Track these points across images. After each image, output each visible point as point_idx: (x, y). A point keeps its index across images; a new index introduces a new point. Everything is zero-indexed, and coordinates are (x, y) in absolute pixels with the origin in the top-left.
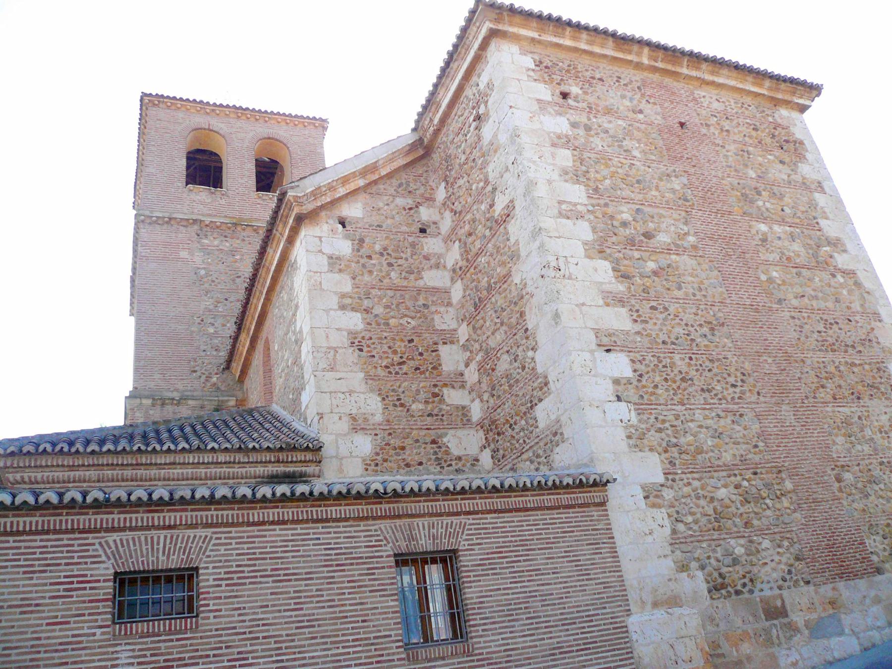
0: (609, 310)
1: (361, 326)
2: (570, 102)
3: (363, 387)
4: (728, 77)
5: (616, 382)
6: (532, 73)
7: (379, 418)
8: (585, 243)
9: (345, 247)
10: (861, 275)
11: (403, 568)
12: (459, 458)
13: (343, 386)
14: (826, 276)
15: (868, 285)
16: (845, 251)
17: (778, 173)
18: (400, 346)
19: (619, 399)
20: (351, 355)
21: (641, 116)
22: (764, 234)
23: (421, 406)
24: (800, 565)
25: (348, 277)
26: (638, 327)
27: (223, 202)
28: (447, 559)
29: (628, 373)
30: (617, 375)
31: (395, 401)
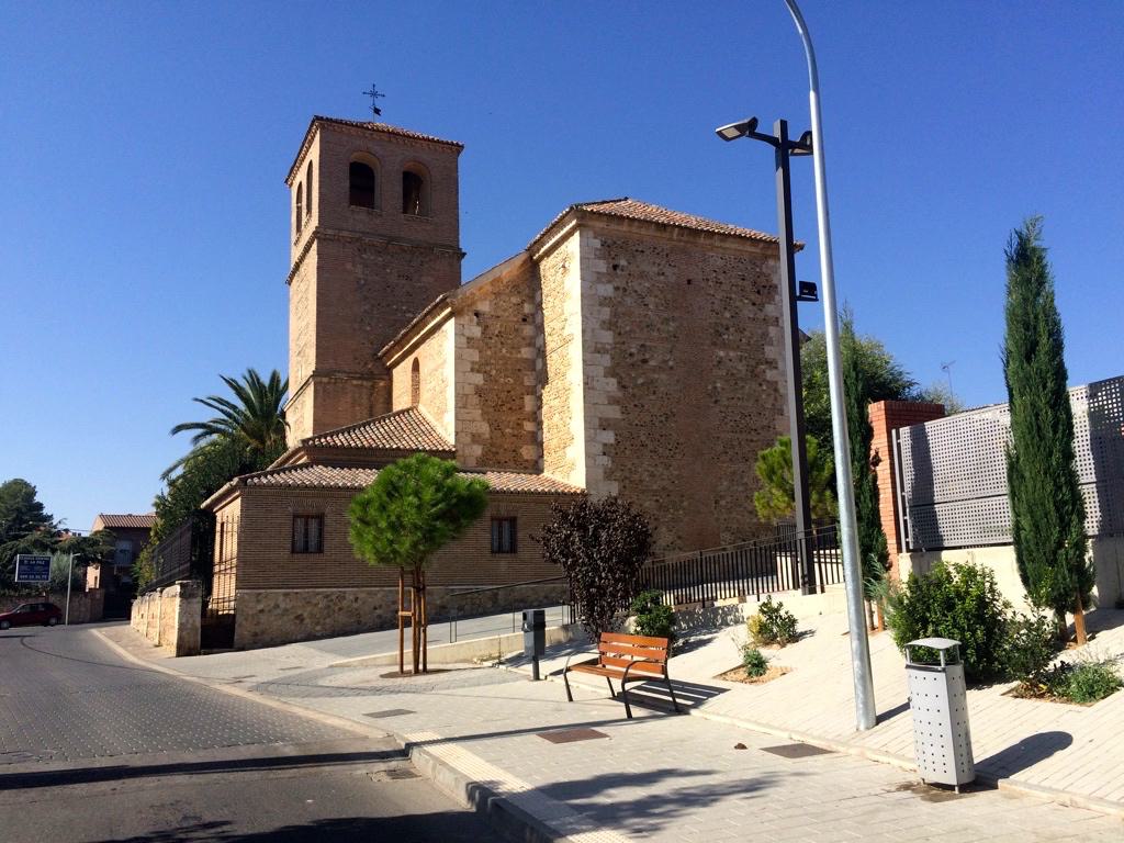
0: (610, 407)
1: (482, 382)
2: (618, 271)
3: (479, 418)
4: (733, 243)
5: (605, 445)
6: (598, 253)
7: (487, 436)
8: (605, 368)
9: (477, 332)
10: (780, 386)
11: (937, 498)
12: (527, 461)
13: (468, 417)
14: (755, 386)
15: (782, 391)
16: (776, 368)
17: (748, 311)
18: (503, 395)
19: (604, 454)
20: (475, 400)
21: (662, 277)
22: (721, 358)
23: (510, 431)
24: (679, 542)
25: (477, 351)
26: (625, 416)
27: (378, 222)
28: (320, 518)
29: (612, 441)
30: (605, 441)
31: (496, 427)
